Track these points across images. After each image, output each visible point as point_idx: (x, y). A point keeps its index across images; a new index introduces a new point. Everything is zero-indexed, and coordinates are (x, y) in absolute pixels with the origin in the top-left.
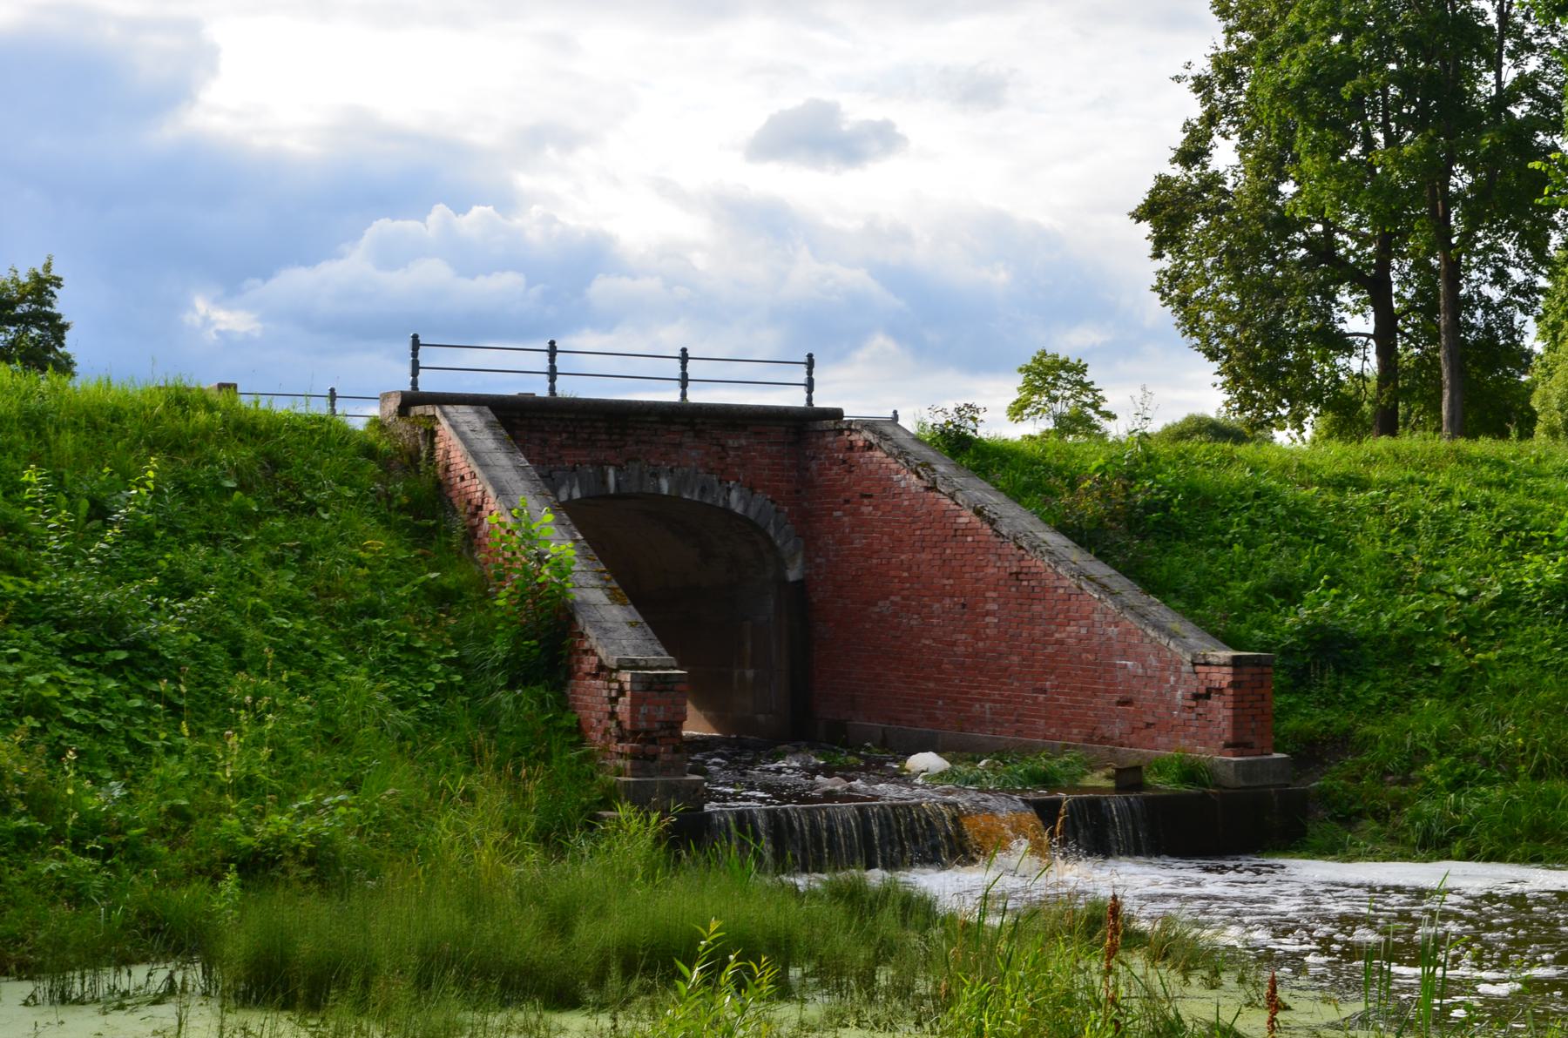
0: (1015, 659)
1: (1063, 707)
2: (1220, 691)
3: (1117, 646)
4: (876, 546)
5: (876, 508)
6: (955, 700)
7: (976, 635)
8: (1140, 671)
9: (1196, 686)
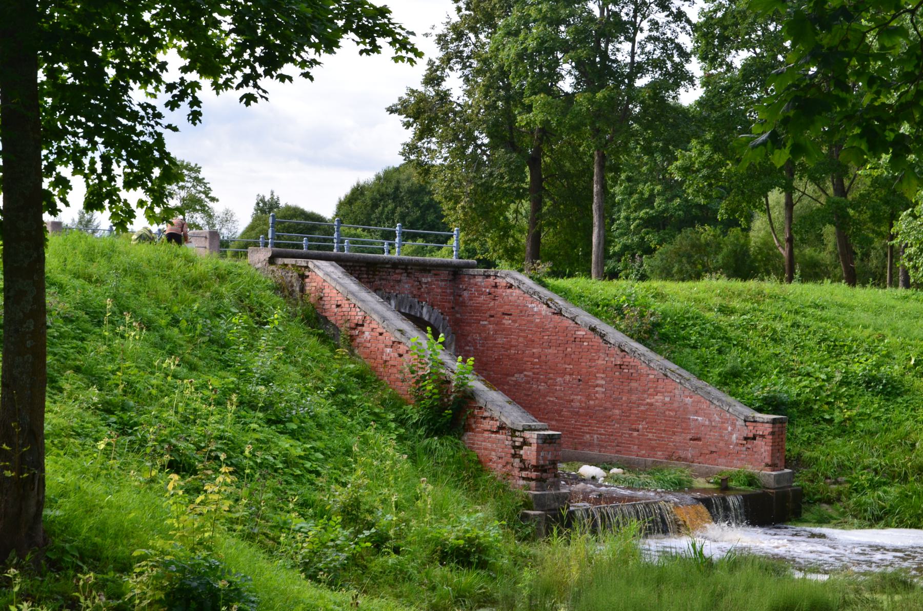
0: (617, 412)
1: (650, 440)
2: (763, 436)
3: (690, 408)
4: (514, 343)
5: (514, 321)
6: (571, 432)
7: (589, 397)
8: (707, 423)
9: (746, 432)
